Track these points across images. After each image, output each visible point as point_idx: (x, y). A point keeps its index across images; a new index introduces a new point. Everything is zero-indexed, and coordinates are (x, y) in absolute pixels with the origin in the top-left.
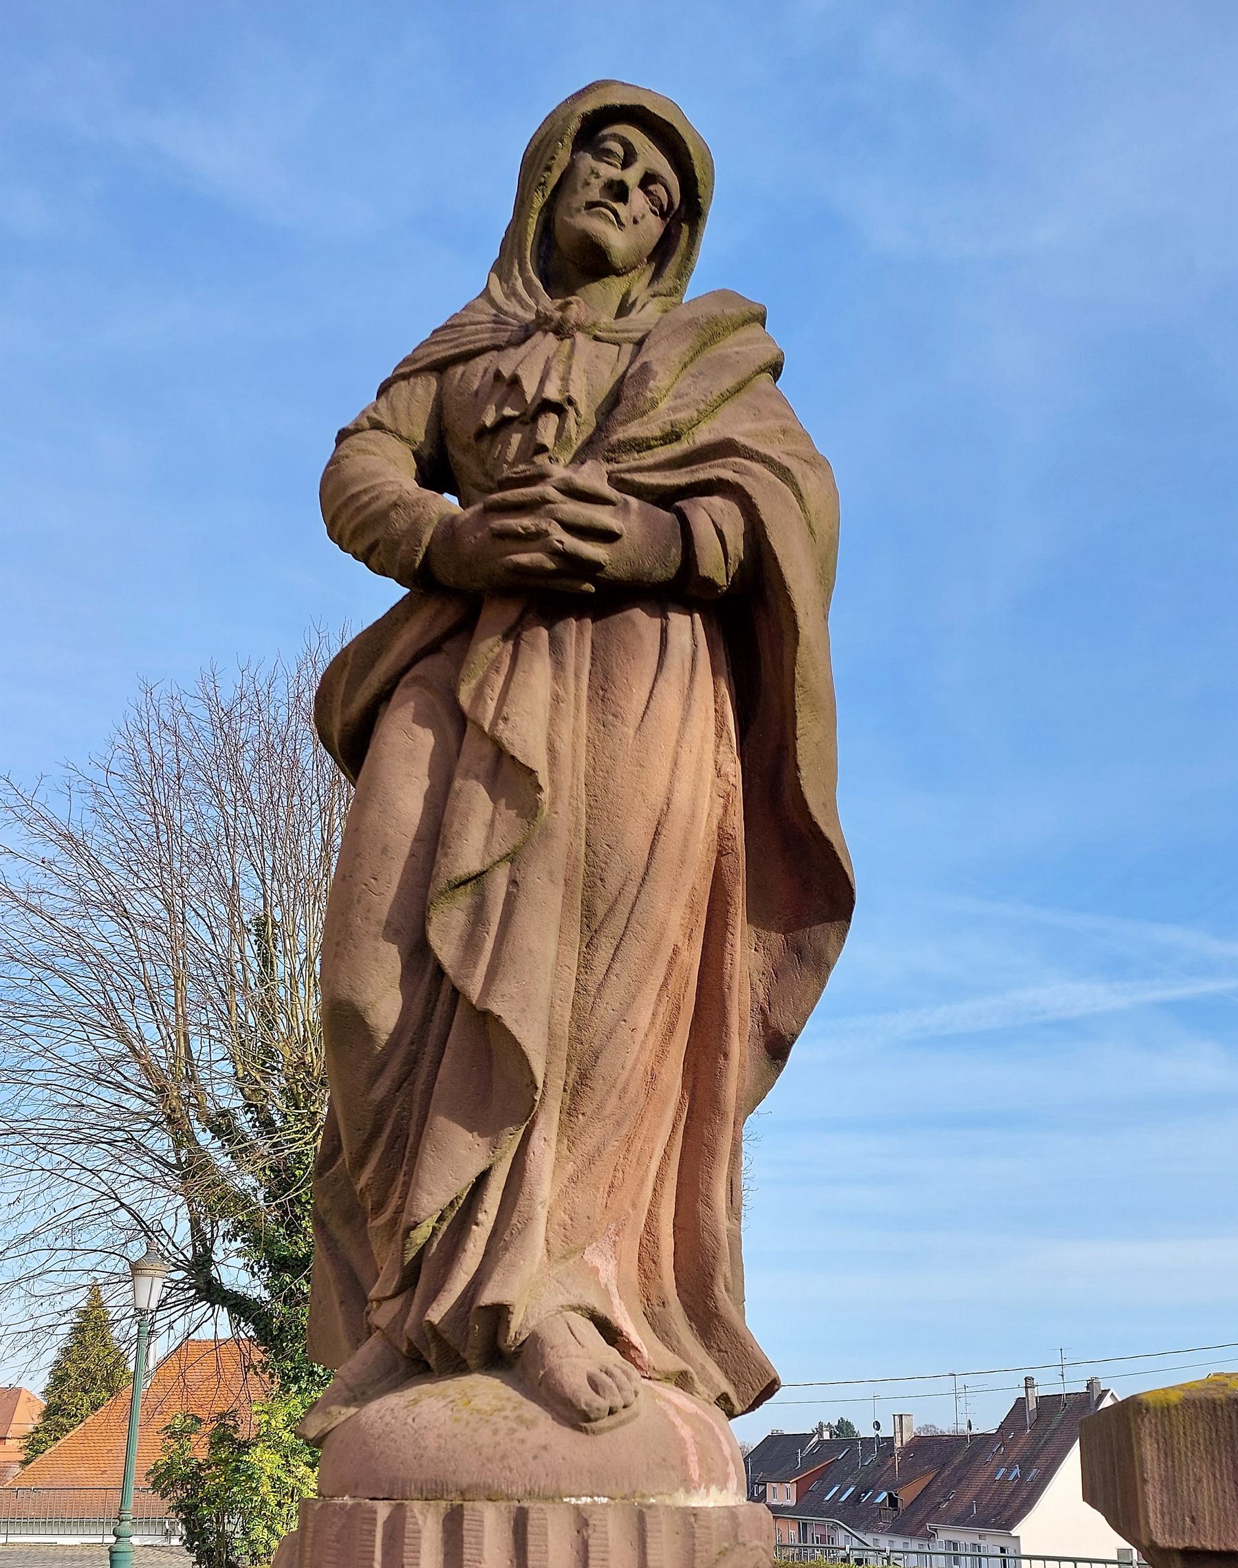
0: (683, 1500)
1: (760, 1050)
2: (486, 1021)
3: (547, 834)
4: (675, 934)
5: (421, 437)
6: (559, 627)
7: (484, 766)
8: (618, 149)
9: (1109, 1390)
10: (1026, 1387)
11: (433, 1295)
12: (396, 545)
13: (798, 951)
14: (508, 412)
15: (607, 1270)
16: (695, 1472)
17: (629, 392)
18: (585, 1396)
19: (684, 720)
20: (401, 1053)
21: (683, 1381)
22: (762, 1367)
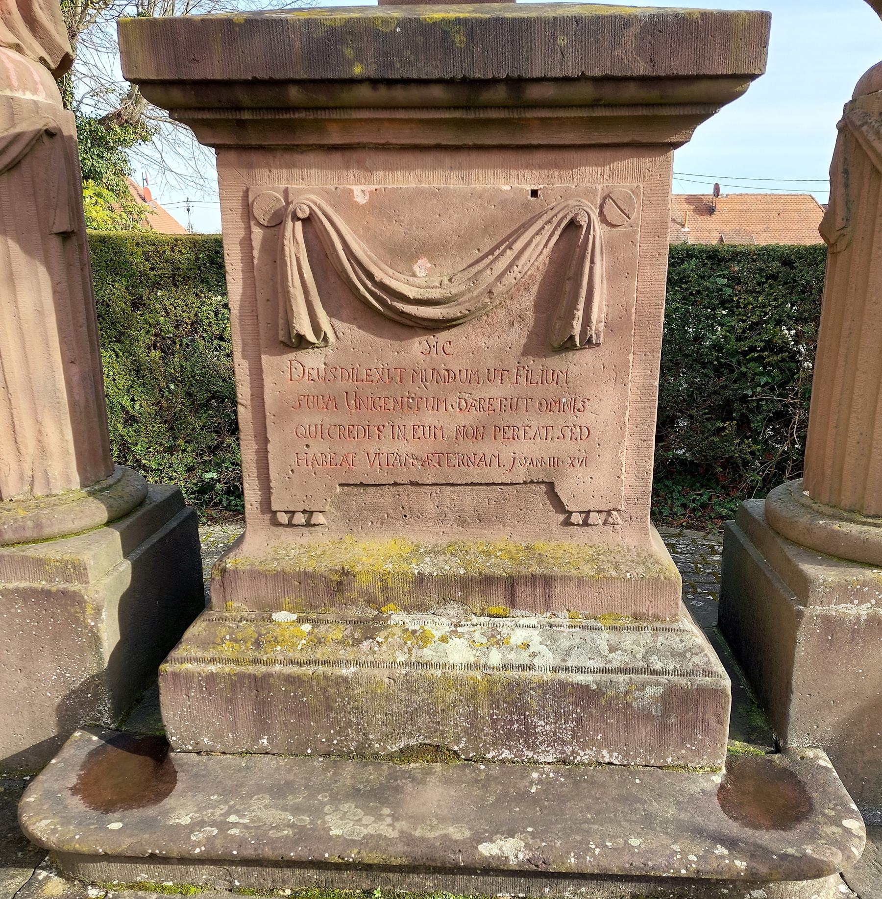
21: (18, 48)
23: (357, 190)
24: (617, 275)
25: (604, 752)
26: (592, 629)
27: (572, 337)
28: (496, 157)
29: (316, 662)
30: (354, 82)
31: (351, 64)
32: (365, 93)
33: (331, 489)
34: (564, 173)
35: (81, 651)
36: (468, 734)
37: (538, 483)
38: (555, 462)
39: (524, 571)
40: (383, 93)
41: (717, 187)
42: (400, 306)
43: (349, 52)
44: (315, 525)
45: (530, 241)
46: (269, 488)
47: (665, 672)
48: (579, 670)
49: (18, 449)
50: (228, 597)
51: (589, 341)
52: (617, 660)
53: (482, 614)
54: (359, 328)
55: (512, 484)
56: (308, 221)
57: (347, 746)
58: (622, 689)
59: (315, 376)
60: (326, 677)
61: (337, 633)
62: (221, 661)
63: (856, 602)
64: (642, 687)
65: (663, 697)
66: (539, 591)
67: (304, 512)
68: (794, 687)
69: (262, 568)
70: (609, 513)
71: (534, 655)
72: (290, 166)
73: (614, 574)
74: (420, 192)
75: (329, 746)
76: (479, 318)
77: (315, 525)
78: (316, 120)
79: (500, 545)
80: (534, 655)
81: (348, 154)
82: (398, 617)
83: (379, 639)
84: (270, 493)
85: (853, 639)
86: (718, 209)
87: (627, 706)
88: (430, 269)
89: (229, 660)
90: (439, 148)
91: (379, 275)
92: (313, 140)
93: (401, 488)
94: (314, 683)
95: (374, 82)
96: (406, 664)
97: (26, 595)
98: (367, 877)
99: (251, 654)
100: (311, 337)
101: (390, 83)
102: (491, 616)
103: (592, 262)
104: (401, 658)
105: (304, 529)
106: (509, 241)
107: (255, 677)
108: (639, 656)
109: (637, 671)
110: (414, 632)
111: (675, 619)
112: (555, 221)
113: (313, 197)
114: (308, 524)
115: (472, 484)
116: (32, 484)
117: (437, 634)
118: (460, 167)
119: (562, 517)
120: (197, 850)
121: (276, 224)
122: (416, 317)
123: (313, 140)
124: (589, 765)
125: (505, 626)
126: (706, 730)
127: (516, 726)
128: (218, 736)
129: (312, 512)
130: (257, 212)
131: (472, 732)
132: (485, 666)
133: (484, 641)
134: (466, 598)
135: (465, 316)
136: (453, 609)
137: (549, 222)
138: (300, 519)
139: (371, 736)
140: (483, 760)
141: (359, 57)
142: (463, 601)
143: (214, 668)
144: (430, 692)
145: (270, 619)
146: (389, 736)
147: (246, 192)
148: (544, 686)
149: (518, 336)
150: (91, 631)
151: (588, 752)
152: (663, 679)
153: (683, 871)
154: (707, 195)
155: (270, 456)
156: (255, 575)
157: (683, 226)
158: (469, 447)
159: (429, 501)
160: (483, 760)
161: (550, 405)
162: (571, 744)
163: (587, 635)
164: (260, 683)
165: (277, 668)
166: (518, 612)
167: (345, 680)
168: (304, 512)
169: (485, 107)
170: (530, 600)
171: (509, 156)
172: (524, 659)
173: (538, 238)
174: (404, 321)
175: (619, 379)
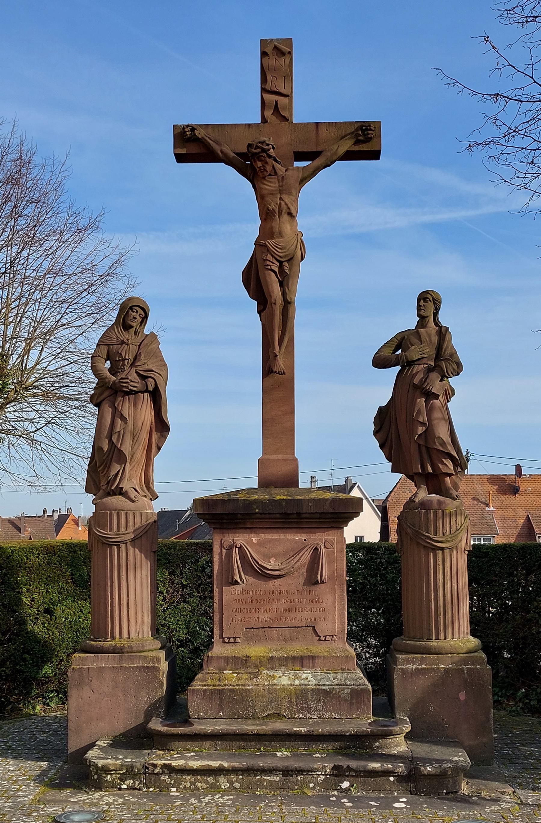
0: (146, 511)
1: (157, 449)
2: (120, 451)
3: (128, 426)
4: (145, 436)
5: (106, 357)
6: (129, 396)
7: (119, 416)
8: (135, 311)
9: (356, 484)
10: (311, 482)
11: (112, 486)
12: (106, 383)
13: (162, 436)
14: (120, 359)
15: (135, 482)
16: (147, 508)
17: (138, 357)
18: (134, 499)
19: (146, 408)
20: (108, 453)
21: (145, 496)
22: (157, 495)
23: (254, 539)
24: (331, 562)
25: (333, 714)
26: (328, 673)
27: (318, 580)
28: (295, 530)
29: (239, 685)
30: (257, 513)
31: (255, 510)
32: (258, 515)
33: (243, 630)
34: (313, 535)
35: (156, 688)
36: (289, 709)
37: (310, 626)
38: (315, 619)
39: (306, 655)
40: (263, 516)
41: (518, 468)
42: (266, 571)
43: (255, 507)
44: (237, 642)
45: (304, 553)
46: (223, 630)
47: (351, 685)
48: (324, 685)
49: (136, 621)
50: (209, 666)
51: (323, 581)
52: (336, 681)
53: (292, 670)
54: (253, 578)
55: (301, 627)
56: (240, 548)
57: (249, 715)
58: (338, 691)
59: (239, 593)
60: (242, 689)
61: (245, 676)
62: (208, 685)
63: (412, 664)
64: (344, 689)
65: (350, 693)
66: (311, 661)
67: (233, 638)
68: (395, 695)
69: (221, 655)
70: (332, 636)
71: (309, 681)
72: (235, 533)
73: (334, 655)
74: (273, 539)
75: (243, 715)
76: (290, 575)
77: (237, 642)
78: (244, 522)
79: (298, 648)
80: (309, 681)
81: (251, 530)
82: (265, 672)
83: (259, 678)
84: (223, 632)
85: (412, 676)
86: (522, 489)
87: (339, 696)
88: (275, 561)
89: (211, 685)
90: (278, 528)
91: (260, 563)
92: (242, 526)
93: (265, 629)
94: (239, 692)
95: (261, 514)
96: (268, 685)
97: (140, 668)
98: (259, 744)
99: (218, 683)
100: (239, 581)
101: (265, 514)
102: (295, 671)
103: (322, 559)
104: (266, 683)
105: (233, 644)
106: (298, 552)
107: (219, 690)
108: (343, 681)
109: (341, 685)
110: (270, 675)
111: (354, 669)
112: (311, 547)
113: (241, 541)
114: (235, 642)
115: (289, 627)
116: (138, 634)
117: (278, 676)
118: (283, 533)
119: (318, 638)
120: (209, 731)
121: (231, 548)
122: (271, 575)
123: (242, 526)
124: (328, 718)
125: (299, 673)
126: (365, 705)
127: (304, 705)
128: (206, 712)
129: (236, 638)
130: (224, 546)
131: (290, 708)
132: (294, 685)
133: (293, 677)
134: (287, 665)
135: (286, 574)
136: (283, 668)
137: (309, 548)
138: (232, 640)
139: (257, 711)
140: (294, 718)
141: (257, 508)
142: (286, 666)
143: (206, 687)
144: (276, 693)
145: (223, 673)
146: (263, 710)
147: (222, 540)
148: (312, 690)
149: (302, 580)
150: (161, 681)
151: (328, 714)
152: (350, 687)
153: (352, 732)
154: (509, 475)
155: (224, 619)
156: (218, 658)
157: (488, 505)
158: (287, 614)
159: (274, 633)
160: (294, 718)
161: (312, 601)
162: (322, 711)
163: (326, 675)
164: (221, 692)
165: (227, 687)
166: (304, 669)
167: (249, 690)
168: (233, 638)
169: (290, 519)
170: (308, 665)
171: (298, 530)
172: (306, 682)
173: (306, 552)
174: (267, 576)
175: (333, 593)
